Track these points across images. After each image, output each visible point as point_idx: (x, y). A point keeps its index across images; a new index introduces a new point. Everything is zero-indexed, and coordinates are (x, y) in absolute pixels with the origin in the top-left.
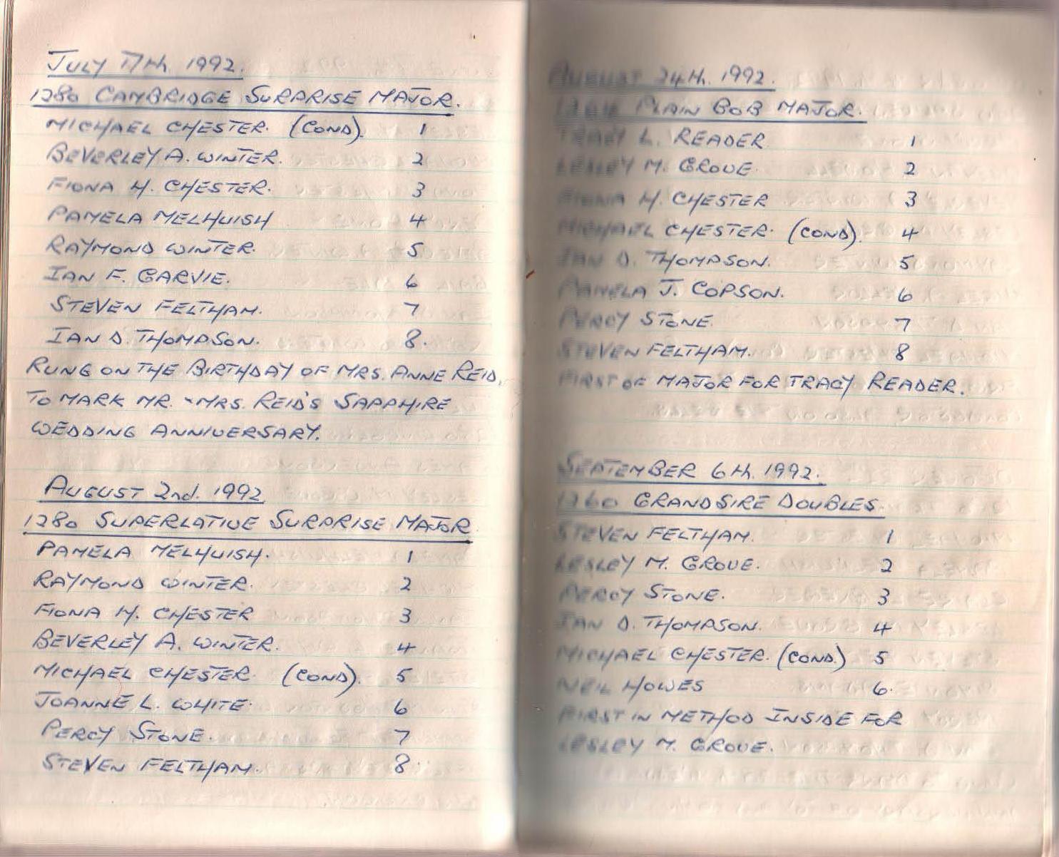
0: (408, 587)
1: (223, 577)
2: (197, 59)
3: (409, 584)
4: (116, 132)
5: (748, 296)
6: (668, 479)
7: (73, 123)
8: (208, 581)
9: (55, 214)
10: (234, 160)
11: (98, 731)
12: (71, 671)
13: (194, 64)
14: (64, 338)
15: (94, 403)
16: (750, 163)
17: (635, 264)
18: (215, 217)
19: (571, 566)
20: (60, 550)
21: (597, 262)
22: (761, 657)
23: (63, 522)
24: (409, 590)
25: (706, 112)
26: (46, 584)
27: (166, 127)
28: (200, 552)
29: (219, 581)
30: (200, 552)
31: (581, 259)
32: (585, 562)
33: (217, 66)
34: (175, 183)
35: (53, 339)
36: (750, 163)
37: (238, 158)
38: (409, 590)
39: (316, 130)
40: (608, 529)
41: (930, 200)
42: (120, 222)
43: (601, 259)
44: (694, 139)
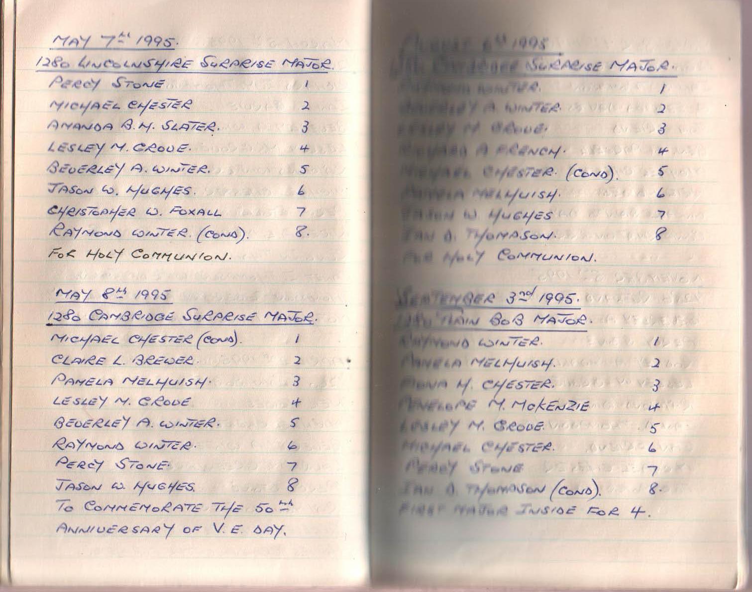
0: (308, 107)
1: (177, 100)
2: (145, 36)
3: (308, 105)
4: (95, 109)
5: (529, 238)
6: (249, 322)
7: (67, 105)
8: (190, 422)
9: (54, 82)
10: (178, 171)
11: (94, 463)
12: (77, 338)
13: (143, 40)
14: (64, 486)
15: (152, 532)
16: (543, 422)
17: (455, 238)
18: (202, 381)
19: (412, 428)
20: (62, 461)
21: (430, 237)
22: (551, 173)
23: (71, 316)
24: (308, 109)
25: (85, 320)
26: (63, 448)
27: (134, 121)
28: (159, 63)
29: (174, 102)
30: (159, 63)
31: (420, 236)
32: (462, 447)
33: (159, 43)
34: (490, 382)
35: (156, 71)
36: (543, 422)
37: (181, 169)
38: (308, 109)
39: (583, 176)
40: (167, 169)
41: (646, 362)
42: (109, 257)
43: (433, 236)
44: (493, 318)
